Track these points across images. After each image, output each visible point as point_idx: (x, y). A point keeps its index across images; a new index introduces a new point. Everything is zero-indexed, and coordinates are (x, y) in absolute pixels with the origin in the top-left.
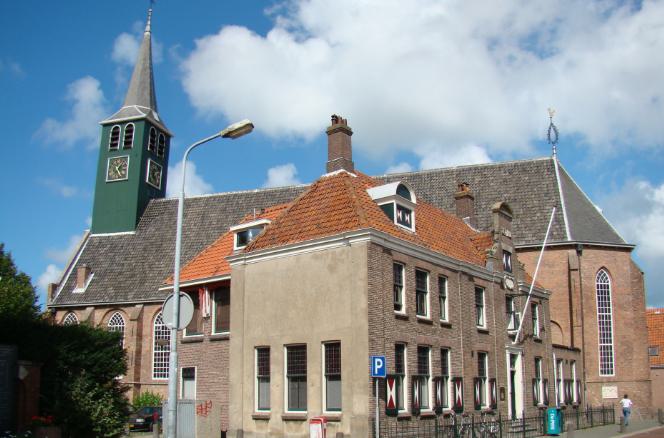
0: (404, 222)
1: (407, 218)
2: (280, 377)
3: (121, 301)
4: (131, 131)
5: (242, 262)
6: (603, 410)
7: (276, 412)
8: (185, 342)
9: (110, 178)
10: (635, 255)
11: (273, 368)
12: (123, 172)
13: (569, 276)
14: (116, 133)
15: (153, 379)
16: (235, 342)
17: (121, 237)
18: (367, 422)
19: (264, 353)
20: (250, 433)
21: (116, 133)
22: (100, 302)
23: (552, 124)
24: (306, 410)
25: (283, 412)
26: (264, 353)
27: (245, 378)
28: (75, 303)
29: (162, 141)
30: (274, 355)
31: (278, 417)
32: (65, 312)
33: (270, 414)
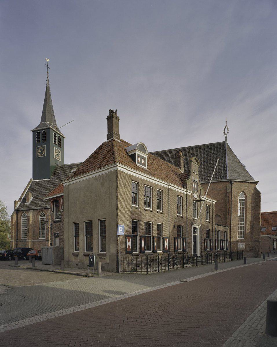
0: (141, 163)
1: (143, 161)
2: (83, 236)
3: (44, 207)
4: (45, 134)
5: (67, 183)
6: (238, 253)
7: (81, 252)
8: (55, 222)
9: (38, 156)
10: (257, 186)
11: (94, 232)
12: (43, 153)
13: (226, 195)
14: (38, 135)
15: (39, 238)
16: (66, 220)
17: (45, 181)
18: (115, 257)
19: (77, 225)
20: (72, 261)
21: (38, 135)
22: (36, 208)
23: (226, 125)
24: (92, 251)
25: (73, 252)
26: (77, 225)
27: (70, 237)
28: (25, 208)
29: (60, 139)
30: (80, 226)
31: (81, 255)
32: (22, 212)
33: (79, 253)
